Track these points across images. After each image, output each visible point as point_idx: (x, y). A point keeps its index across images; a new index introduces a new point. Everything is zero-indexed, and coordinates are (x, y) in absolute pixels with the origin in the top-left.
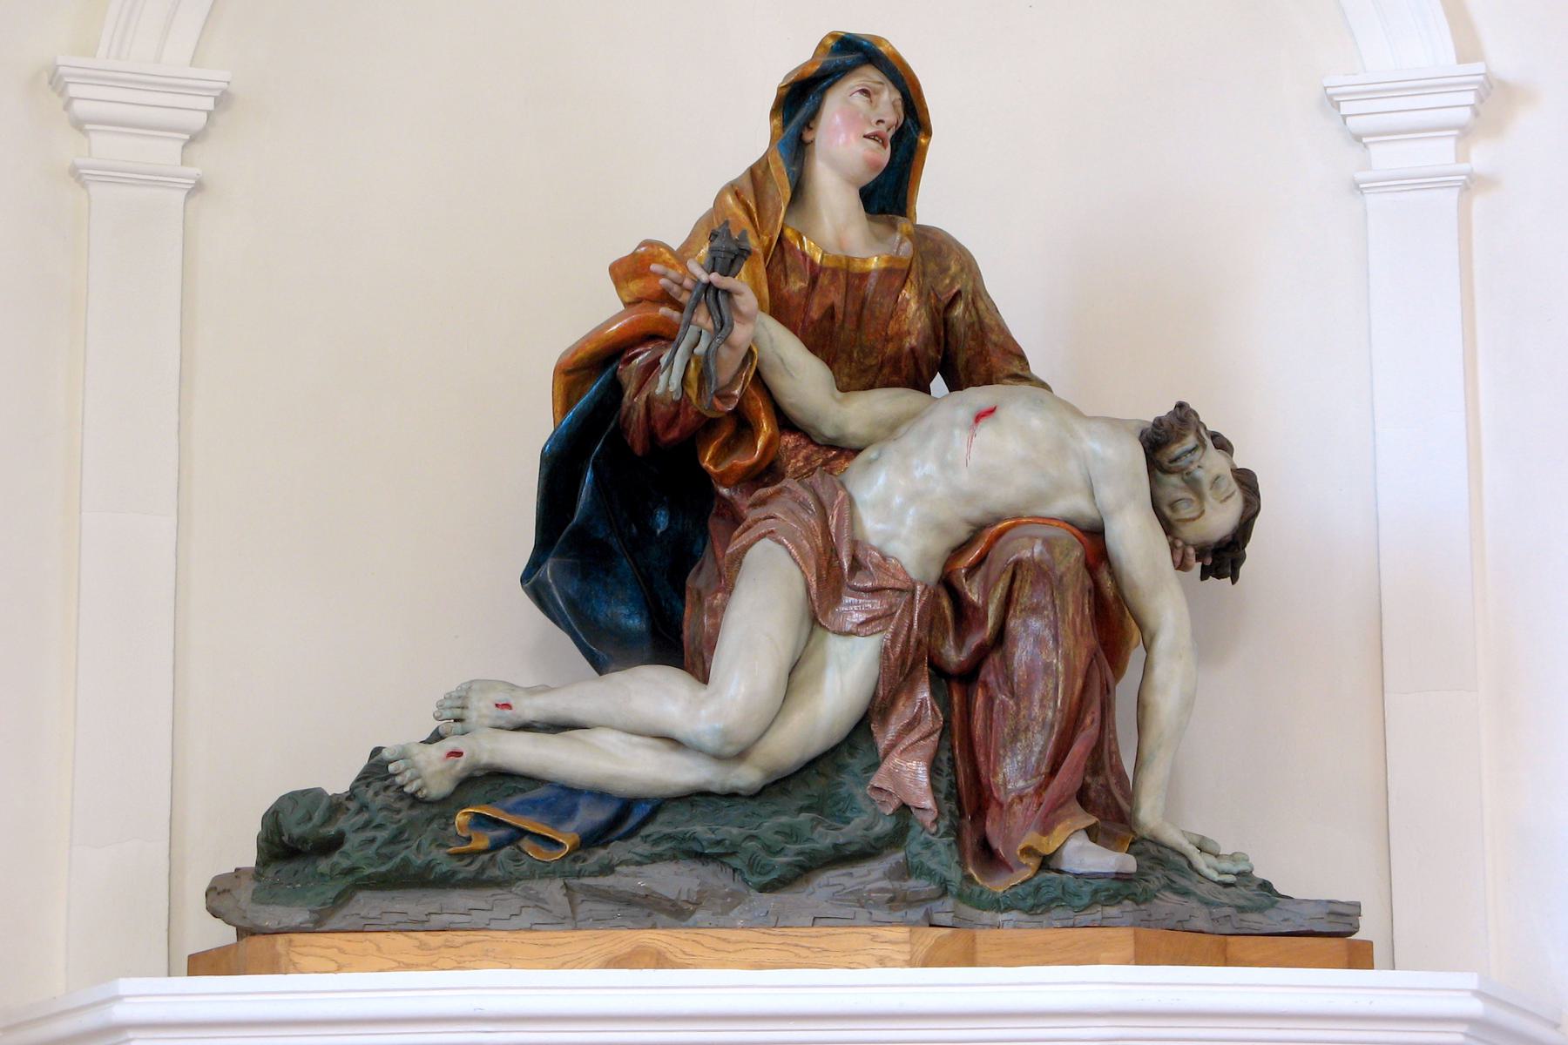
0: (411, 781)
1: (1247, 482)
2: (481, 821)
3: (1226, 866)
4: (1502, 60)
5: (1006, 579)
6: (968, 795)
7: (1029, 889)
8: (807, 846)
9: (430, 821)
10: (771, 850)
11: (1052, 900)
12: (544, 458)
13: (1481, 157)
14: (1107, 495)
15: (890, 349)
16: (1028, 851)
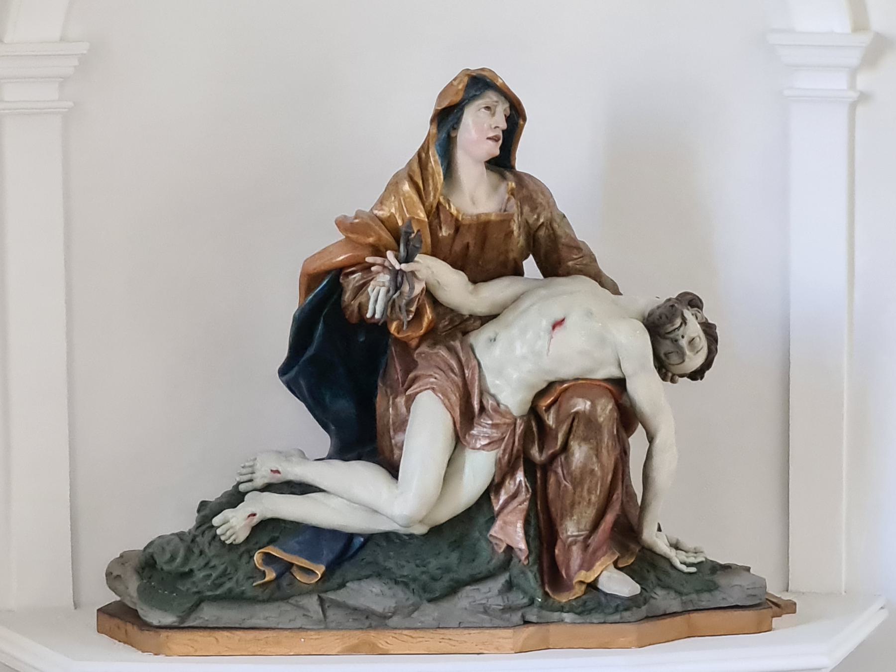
0: (229, 538)
1: (709, 330)
2: (269, 559)
3: (692, 560)
4: (878, 21)
5: (570, 421)
6: (543, 528)
7: (581, 602)
8: (456, 576)
9: (241, 556)
10: (434, 579)
11: (592, 609)
12: (295, 319)
13: (863, 81)
14: (628, 369)
15: (502, 258)
16: (582, 582)
